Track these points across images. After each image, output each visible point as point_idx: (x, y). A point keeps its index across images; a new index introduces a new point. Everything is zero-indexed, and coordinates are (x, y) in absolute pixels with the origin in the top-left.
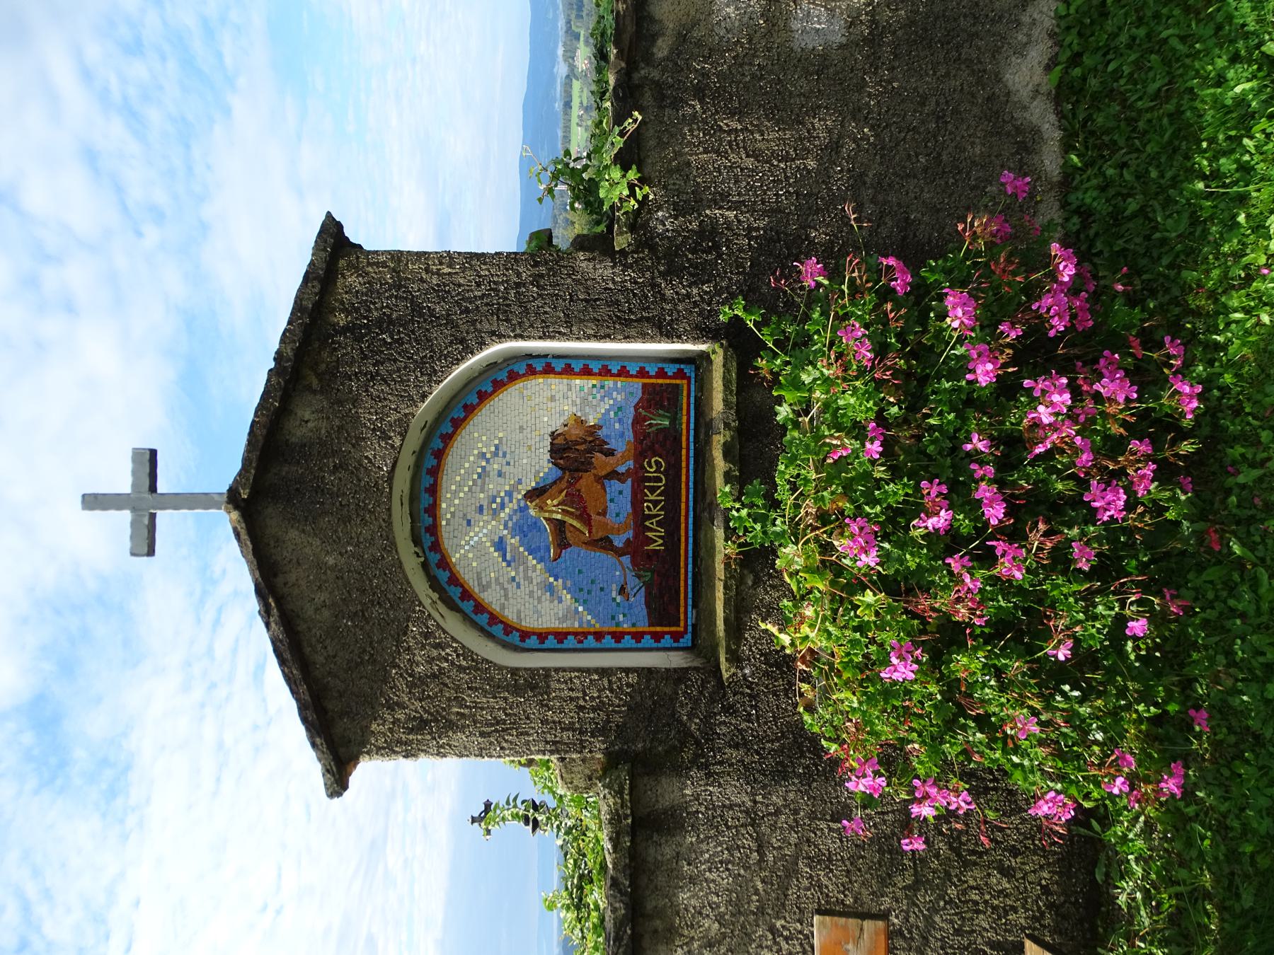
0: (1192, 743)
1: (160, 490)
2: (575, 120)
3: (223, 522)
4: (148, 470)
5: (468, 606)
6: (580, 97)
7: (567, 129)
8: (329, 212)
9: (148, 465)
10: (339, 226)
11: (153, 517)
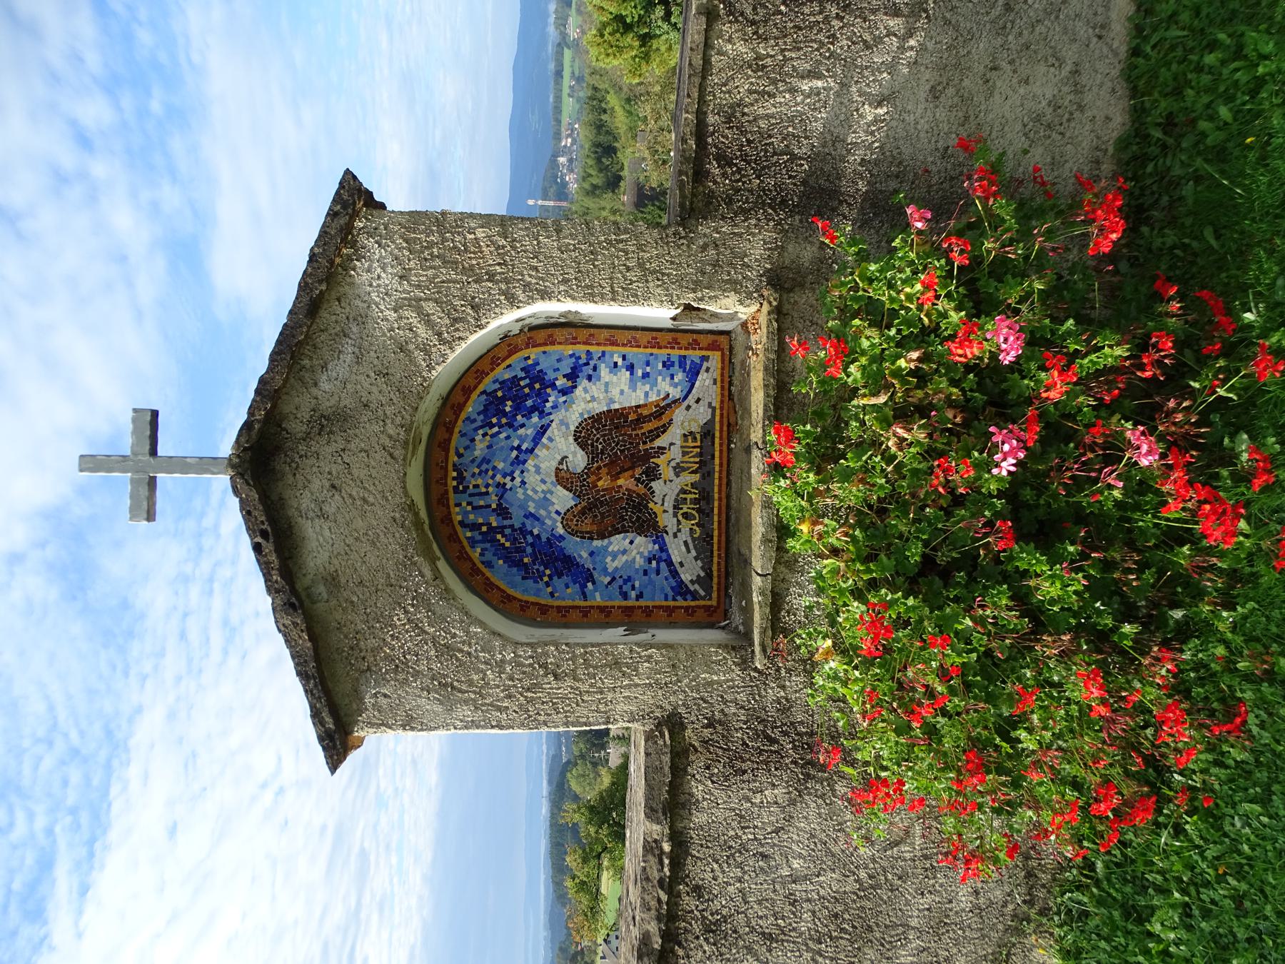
0: (1102, 605)
1: (159, 454)
2: (566, 91)
3: (222, 481)
4: (148, 433)
5: (647, 337)
6: (572, 66)
7: (558, 99)
8: (348, 172)
9: (148, 427)
10: (355, 178)
11: (152, 482)
